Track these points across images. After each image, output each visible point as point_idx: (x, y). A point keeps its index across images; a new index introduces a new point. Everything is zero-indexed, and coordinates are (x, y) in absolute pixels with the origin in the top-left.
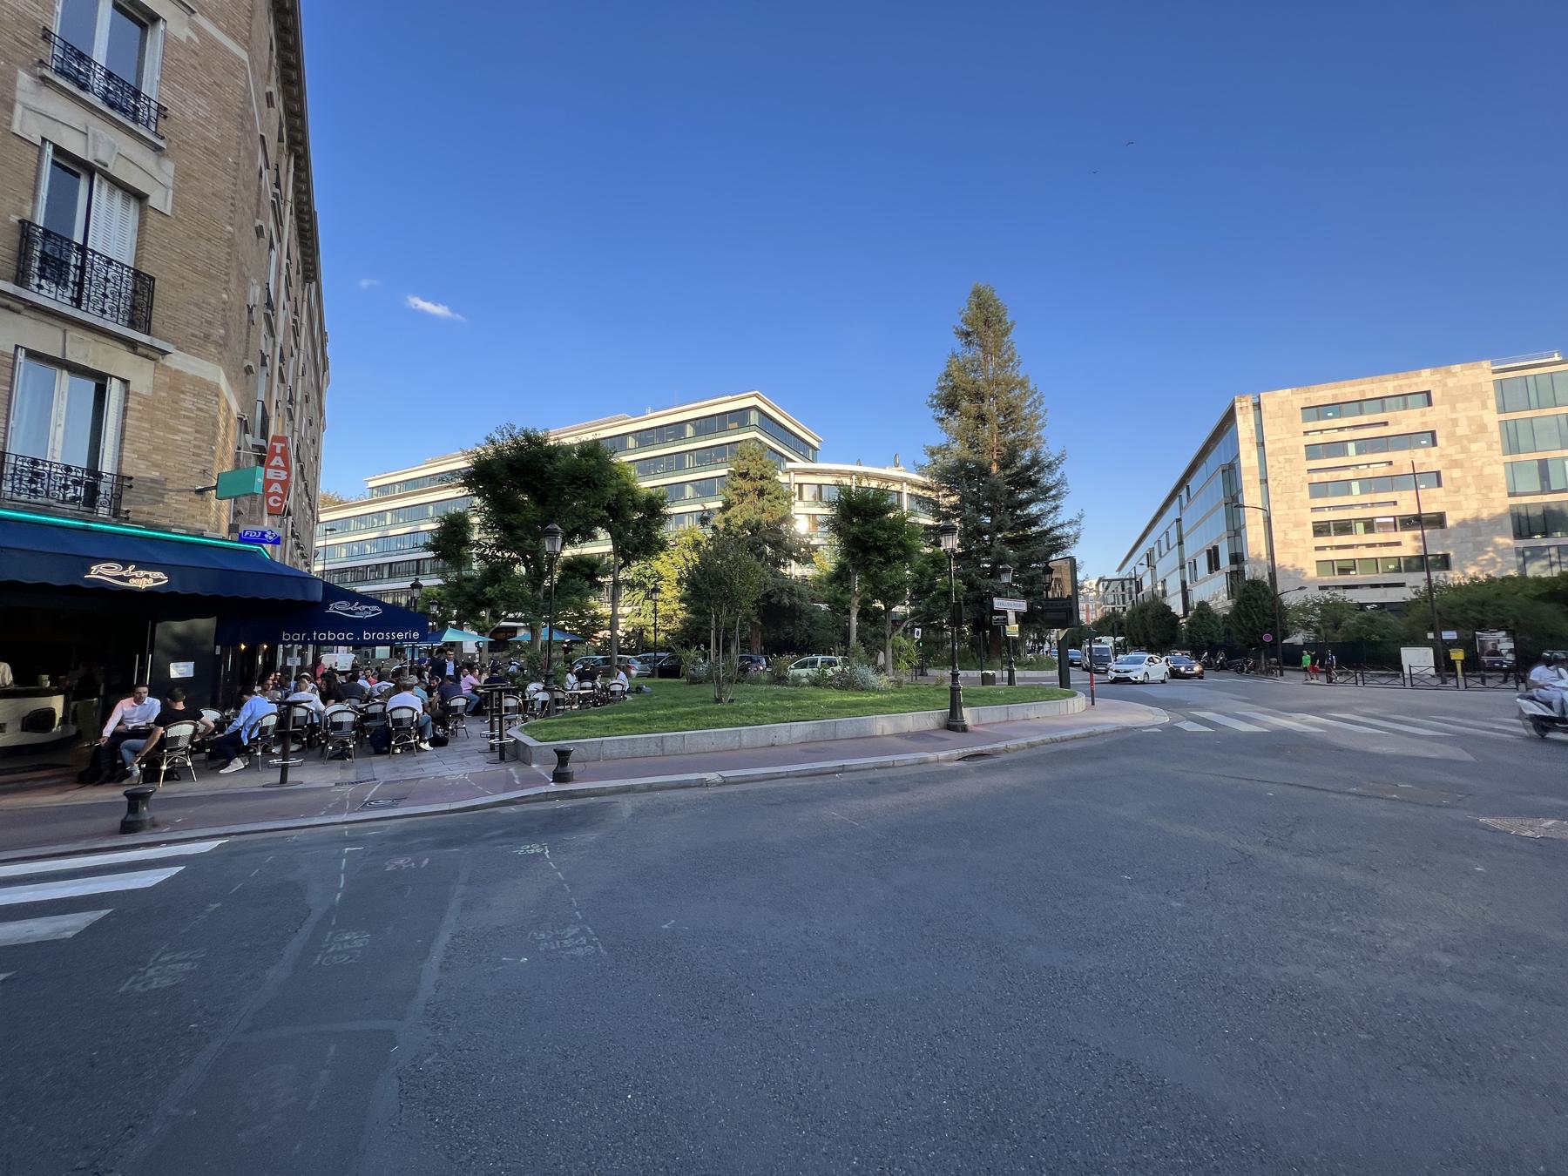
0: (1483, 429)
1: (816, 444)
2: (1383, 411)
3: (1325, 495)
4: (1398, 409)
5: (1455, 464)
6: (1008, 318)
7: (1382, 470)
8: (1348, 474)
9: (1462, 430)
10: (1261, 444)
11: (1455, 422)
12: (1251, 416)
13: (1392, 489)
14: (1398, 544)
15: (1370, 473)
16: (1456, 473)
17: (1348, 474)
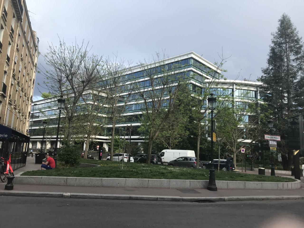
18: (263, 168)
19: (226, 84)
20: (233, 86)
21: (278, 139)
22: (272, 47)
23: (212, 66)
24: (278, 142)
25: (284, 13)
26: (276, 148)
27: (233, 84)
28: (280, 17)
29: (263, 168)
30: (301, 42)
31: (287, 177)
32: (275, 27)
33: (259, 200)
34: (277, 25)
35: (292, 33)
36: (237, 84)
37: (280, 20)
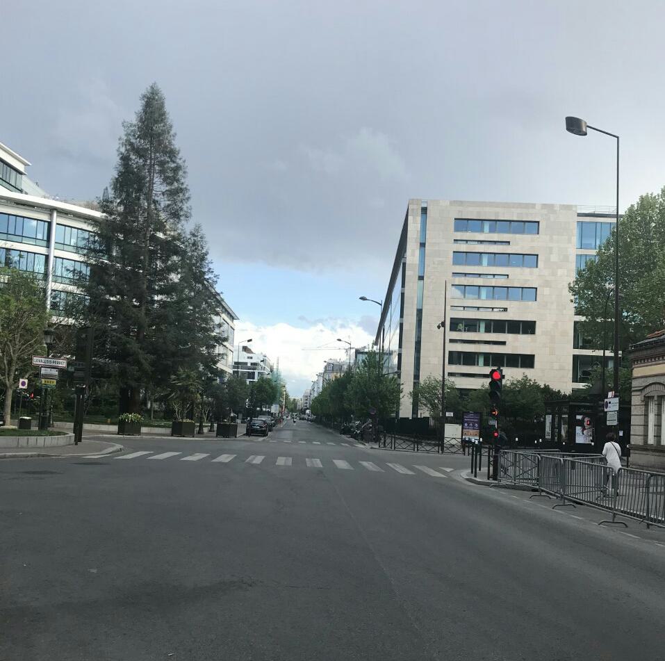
0: (566, 259)
1: (21, 167)
2: (507, 298)
3: (467, 263)
4: (518, 266)
5: (547, 284)
6: (177, 149)
7: (501, 282)
8: (479, 281)
9: (554, 258)
10: (423, 245)
11: (551, 250)
12: (419, 219)
13: (508, 264)
14: (503, 343)
15: (493, 282)
16: (546, 291)
17: (479, 281)
18: (28, 418)
19: (34, 207)
20: (51, 215)
21: (60, 365)
22: (122, 154)
23: (15, 161)
24: (61, 370)
25: (155, 83)
26: (55, 381)
27: (51, 210)
28: (144, 89)
29: (28, 418)
30: (180, 159)
31: (104, 436)
32: (131, 113)
33: (404, 290)
34: (139, 106)
35: (163, 132)
36: (63, 213)
37: (144, 96)
